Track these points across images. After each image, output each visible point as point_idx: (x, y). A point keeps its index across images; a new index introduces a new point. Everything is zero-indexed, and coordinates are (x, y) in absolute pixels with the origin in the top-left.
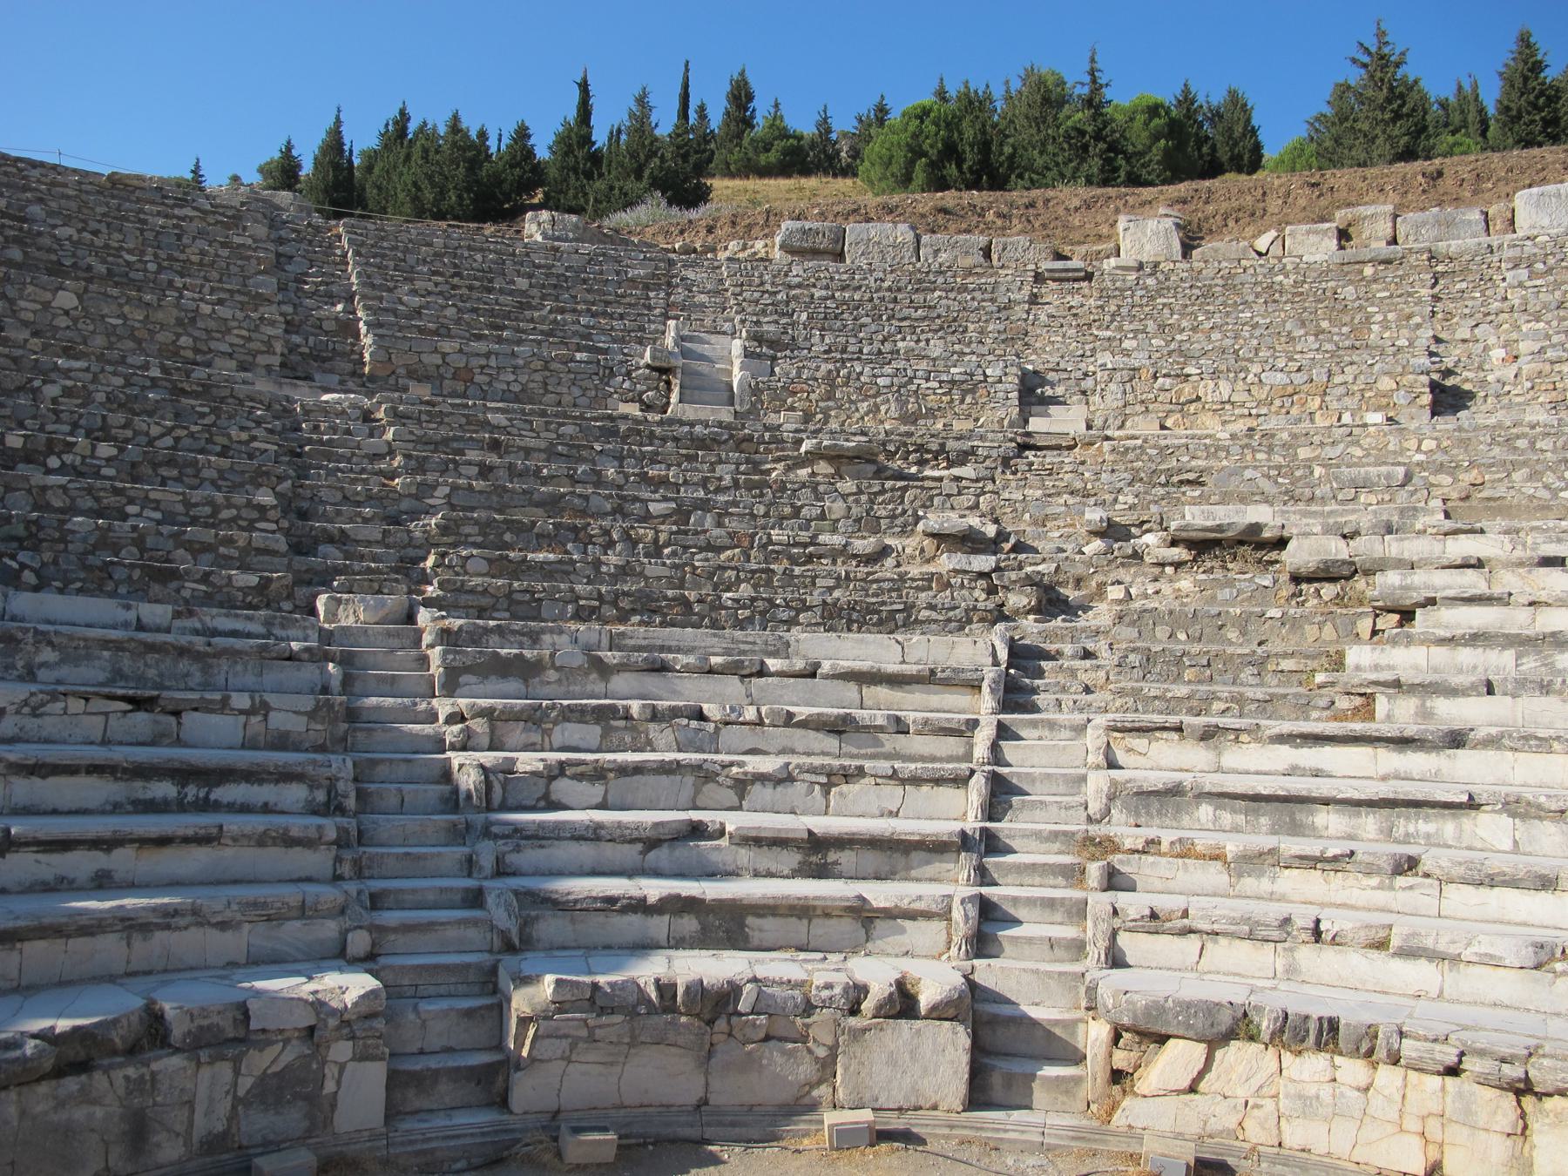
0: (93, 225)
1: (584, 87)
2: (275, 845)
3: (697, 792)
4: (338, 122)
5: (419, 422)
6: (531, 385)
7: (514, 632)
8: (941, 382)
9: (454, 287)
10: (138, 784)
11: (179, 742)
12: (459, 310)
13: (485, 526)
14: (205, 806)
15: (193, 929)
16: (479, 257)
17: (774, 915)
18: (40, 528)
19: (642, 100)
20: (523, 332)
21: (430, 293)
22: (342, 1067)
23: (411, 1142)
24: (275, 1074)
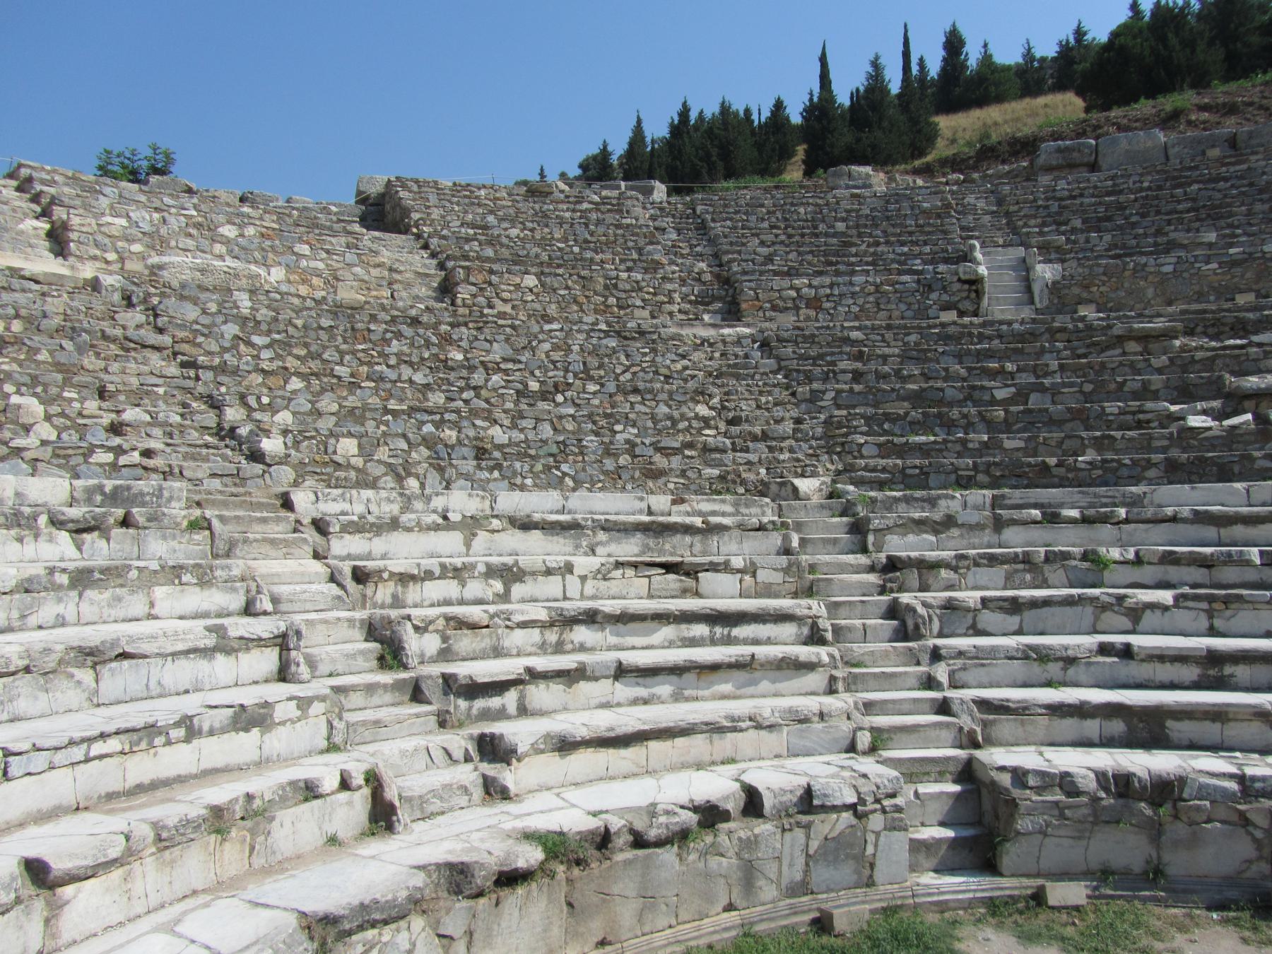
0: (529, 225)
1: (823, 60)
2: (788, 668)
3: (1097, 618)
4: (639, 121)
5: (797, 343)
6: (868, 306)
7: (917, 499)
8: (1220, 263)
9: (790, 236)
10: (684, 626)
11: (697, 594)
12: (800, 254)
13: (868, 419)
14: (729, 641)
15: (751, 731)
16: (802, 210)
17: (1190, 719)
18: (566, 446)
19: (875, 64)
20: (853, 264)
21: (774, 243)
22: (878, 834)
23: (930, 894)
24: (833, 838)
